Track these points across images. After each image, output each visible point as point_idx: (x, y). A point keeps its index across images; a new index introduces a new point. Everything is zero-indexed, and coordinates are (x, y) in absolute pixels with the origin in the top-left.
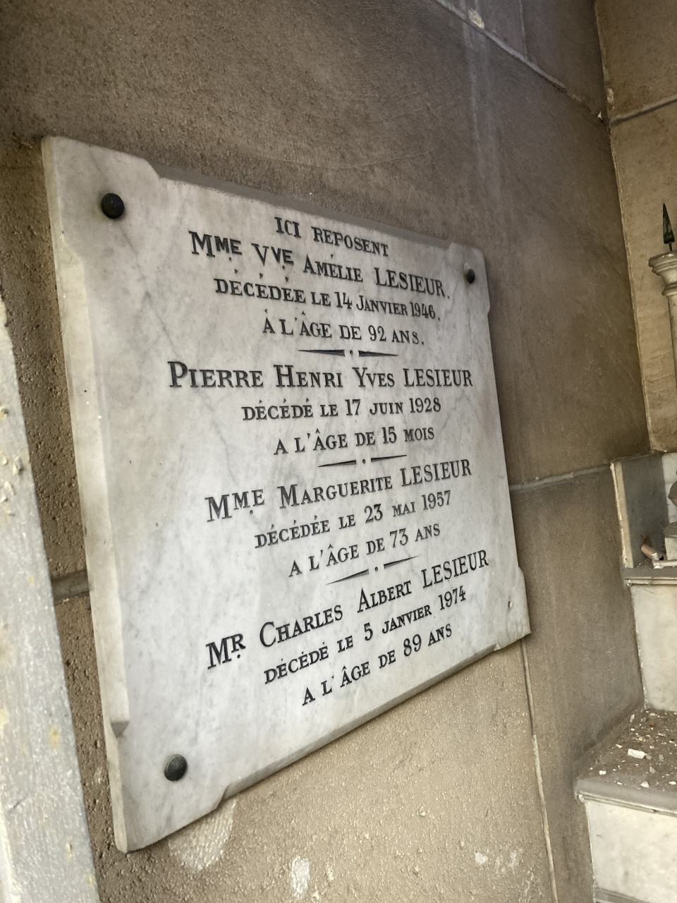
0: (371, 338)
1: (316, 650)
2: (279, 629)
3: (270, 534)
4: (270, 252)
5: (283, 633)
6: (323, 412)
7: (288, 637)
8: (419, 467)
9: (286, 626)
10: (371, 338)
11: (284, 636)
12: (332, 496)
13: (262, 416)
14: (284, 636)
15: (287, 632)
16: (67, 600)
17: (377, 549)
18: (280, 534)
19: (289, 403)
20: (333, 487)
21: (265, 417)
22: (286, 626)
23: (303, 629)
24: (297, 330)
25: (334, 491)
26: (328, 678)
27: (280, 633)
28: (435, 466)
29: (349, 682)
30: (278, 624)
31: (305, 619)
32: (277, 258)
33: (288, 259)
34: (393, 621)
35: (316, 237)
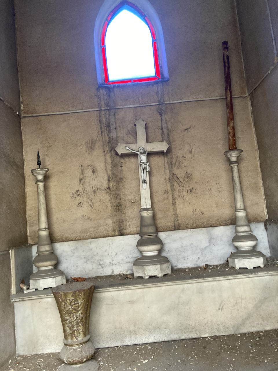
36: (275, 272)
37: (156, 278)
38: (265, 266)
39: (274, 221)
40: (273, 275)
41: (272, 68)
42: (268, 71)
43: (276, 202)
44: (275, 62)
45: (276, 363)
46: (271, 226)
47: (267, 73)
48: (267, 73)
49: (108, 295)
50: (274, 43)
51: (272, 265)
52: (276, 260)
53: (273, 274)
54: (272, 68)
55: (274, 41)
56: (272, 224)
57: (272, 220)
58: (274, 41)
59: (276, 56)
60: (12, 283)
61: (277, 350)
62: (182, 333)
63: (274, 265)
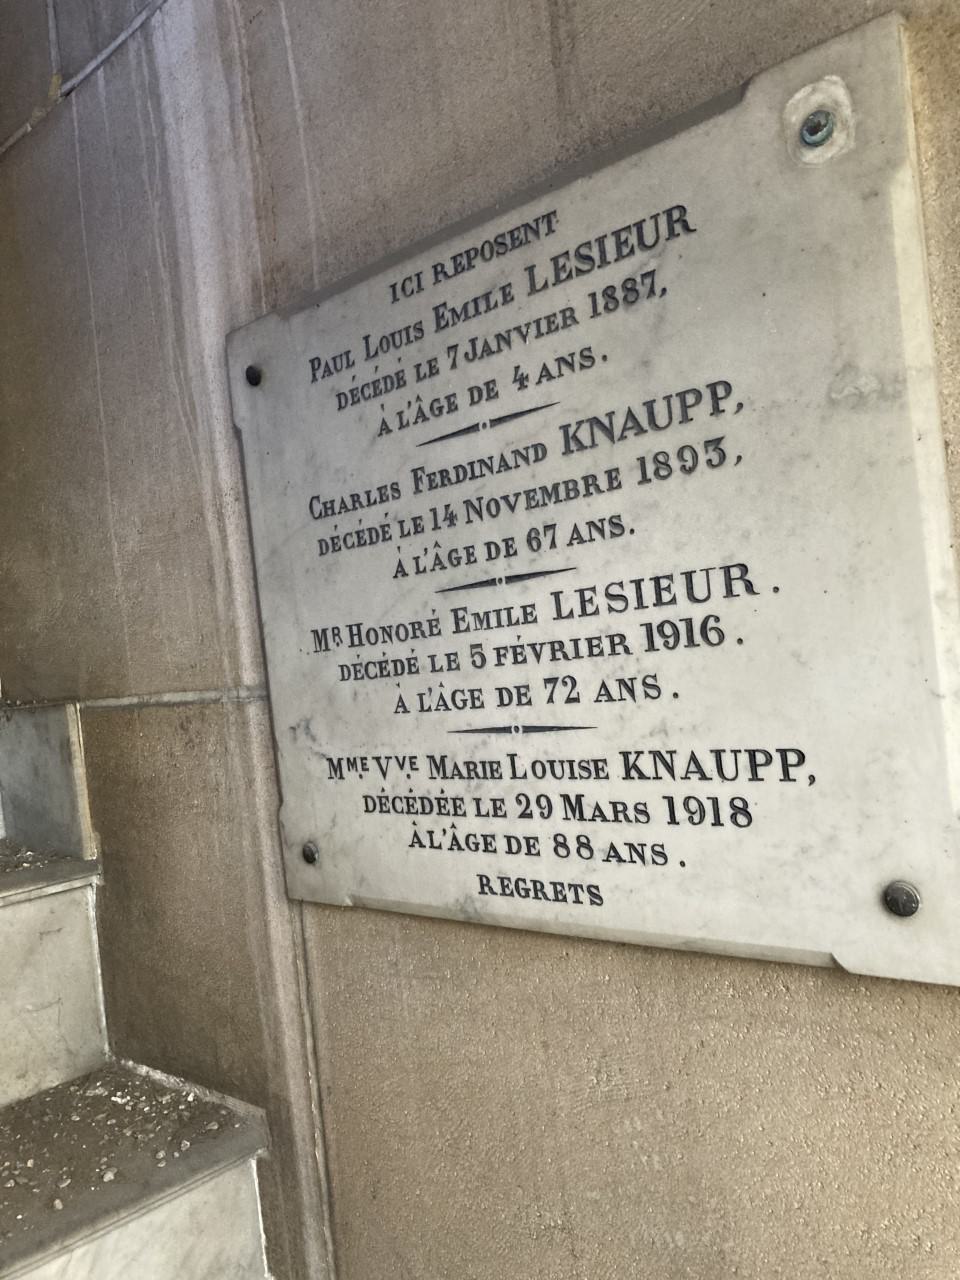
0: (474, 663)
1: (474, 760)
2: (325, 504)
3: (354, 666)
4: (393, 762)
5: (329, 510)
6: (478, 809)
7: (333, 513)
8: (593, 589)
9: (332, 502)
10: (474, 663)
11: (330, 512)
12: (460, 704)
13: (359, 676)
14: (330, 512)
15: (332, 508)
16: (101, 1143)
17: (350, 402)
18: (366, 670)
19: (417, 794)
20: (463, 692)
21: (362, 678)
22: (332, 502)
23: (350, 506)
24: (447, 842)
25: (463, 698)
26: (421, 553)
27: (326, 509)
28: (638, 583)
29: (331, 373)
30: (322, 500)
31: (352, 496)
32: (402, 766)
33: (414, 767)
34: (502, 458)
35: (482, 888)
36: (20, 891)
37: (671, 778)
38: (197, 1141)
39: (25, 704)
40: (13, 904)
41: (38, 113)
42: (24, 123)
43: (37, 630)
44: (51, 93)
45: (10, 1235)
46: (12, 722)
47: (20, 133)
48: (20, 133)
49: (637, 763)
50: (51, 23)
51: (10, 867)
52: (24, 849)
53: (13, 899)
54: (38, 113)
55: (51, 11)
56: (16, 717)
57: (18, 703)
58: (51, 11)
59: (55, 72)
60: (88, 811)
61: (12, 1181)
62: (797, 13)
63: (16, 867)
